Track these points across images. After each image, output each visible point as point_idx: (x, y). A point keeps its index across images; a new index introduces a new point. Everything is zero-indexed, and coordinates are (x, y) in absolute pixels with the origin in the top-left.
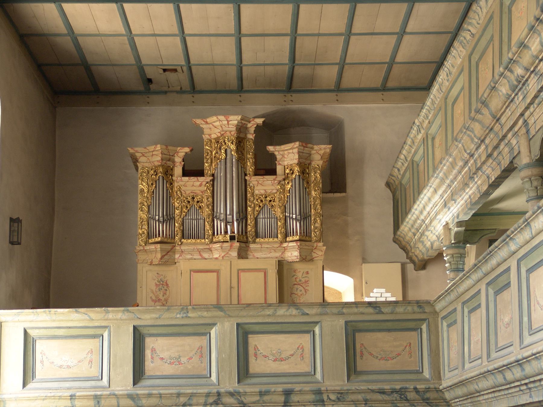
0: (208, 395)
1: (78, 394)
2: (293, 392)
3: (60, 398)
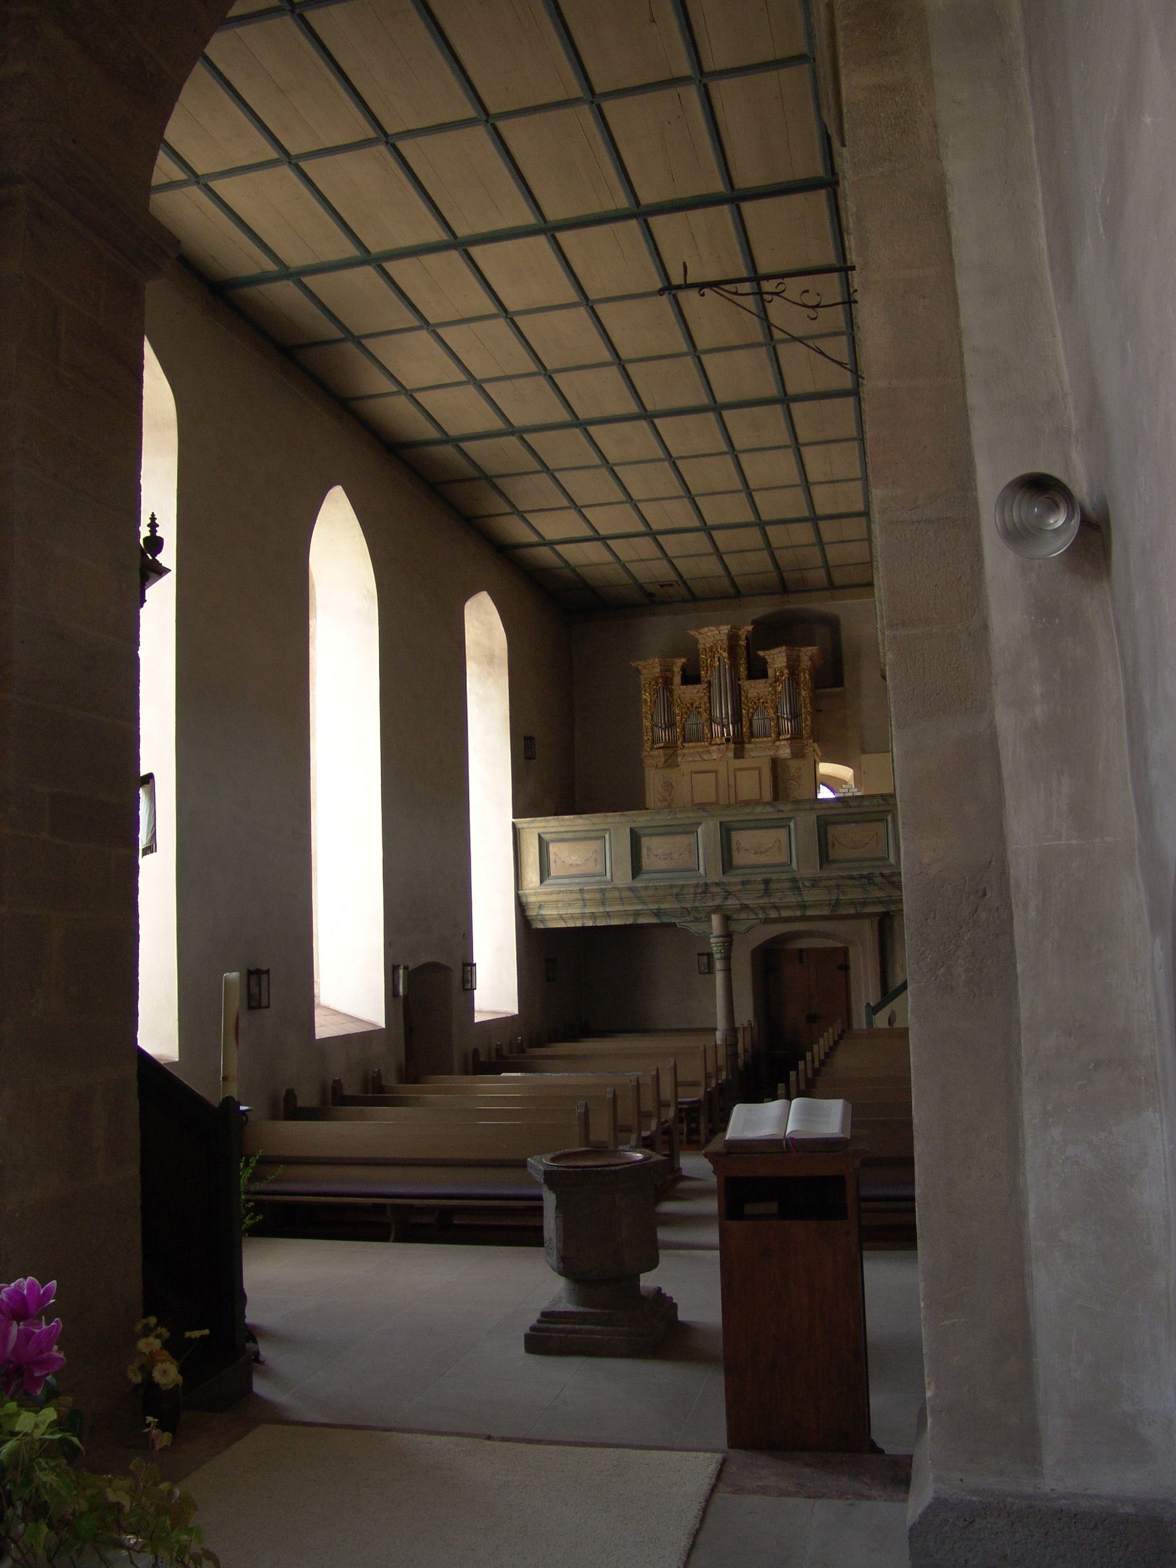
0: (697, 886)
1: (585, 888)
3: (571, 892)
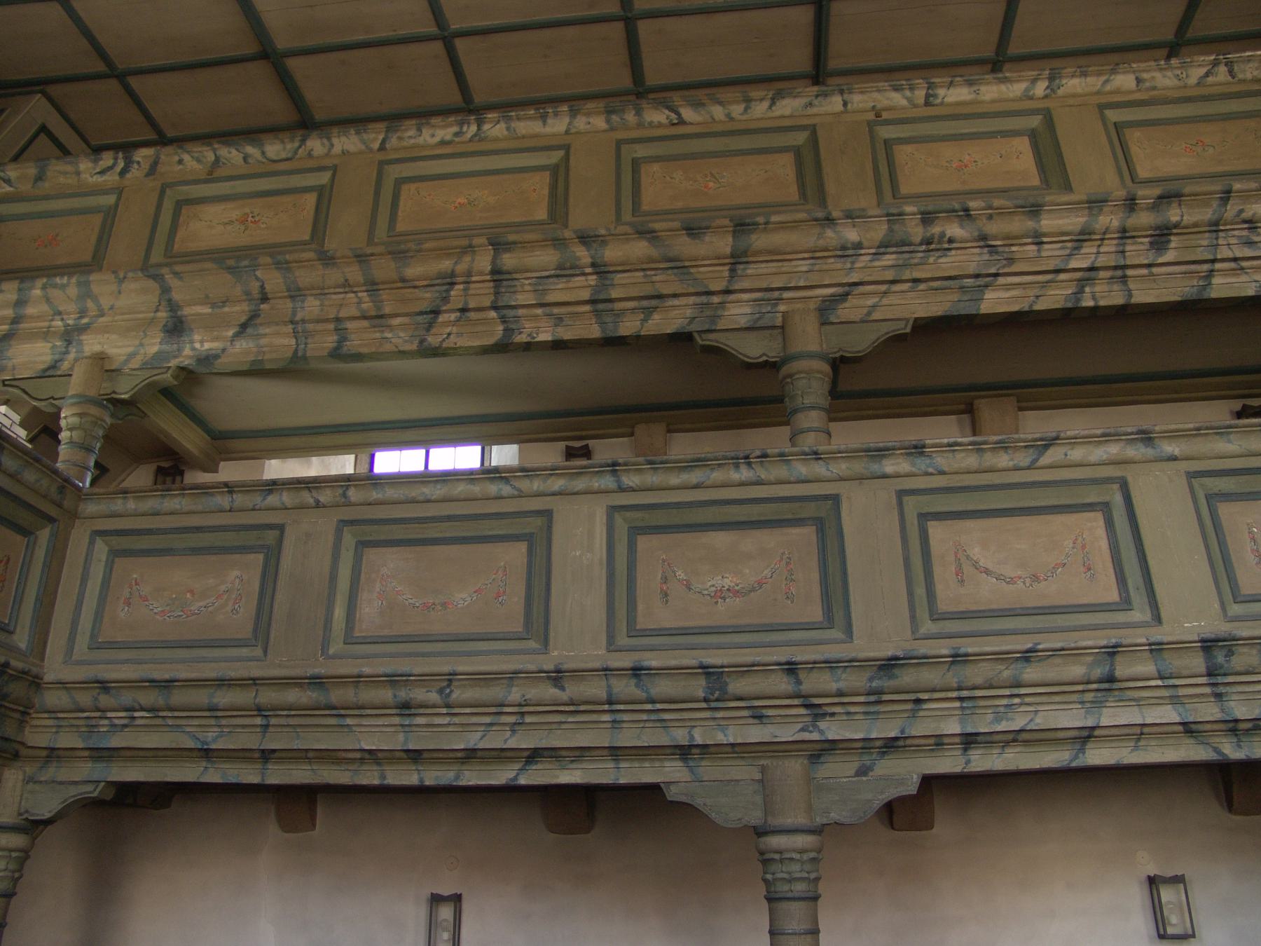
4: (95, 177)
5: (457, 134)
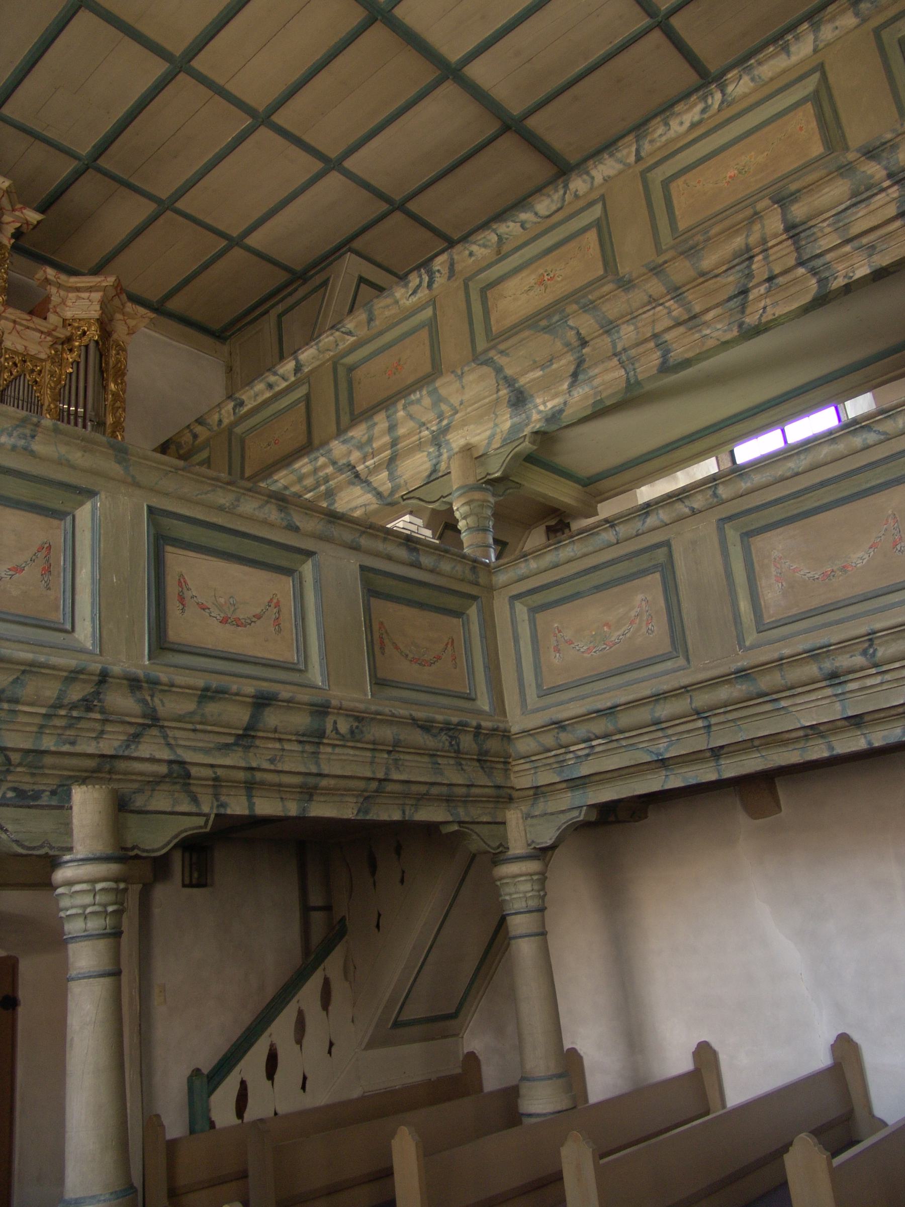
2: (274, 702)
4: (410, 299)
5: (703, 111)
